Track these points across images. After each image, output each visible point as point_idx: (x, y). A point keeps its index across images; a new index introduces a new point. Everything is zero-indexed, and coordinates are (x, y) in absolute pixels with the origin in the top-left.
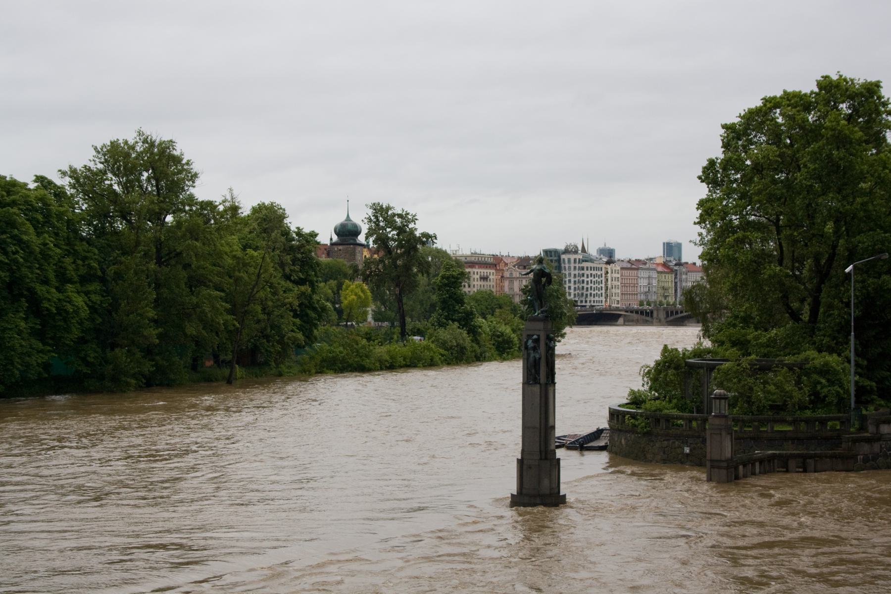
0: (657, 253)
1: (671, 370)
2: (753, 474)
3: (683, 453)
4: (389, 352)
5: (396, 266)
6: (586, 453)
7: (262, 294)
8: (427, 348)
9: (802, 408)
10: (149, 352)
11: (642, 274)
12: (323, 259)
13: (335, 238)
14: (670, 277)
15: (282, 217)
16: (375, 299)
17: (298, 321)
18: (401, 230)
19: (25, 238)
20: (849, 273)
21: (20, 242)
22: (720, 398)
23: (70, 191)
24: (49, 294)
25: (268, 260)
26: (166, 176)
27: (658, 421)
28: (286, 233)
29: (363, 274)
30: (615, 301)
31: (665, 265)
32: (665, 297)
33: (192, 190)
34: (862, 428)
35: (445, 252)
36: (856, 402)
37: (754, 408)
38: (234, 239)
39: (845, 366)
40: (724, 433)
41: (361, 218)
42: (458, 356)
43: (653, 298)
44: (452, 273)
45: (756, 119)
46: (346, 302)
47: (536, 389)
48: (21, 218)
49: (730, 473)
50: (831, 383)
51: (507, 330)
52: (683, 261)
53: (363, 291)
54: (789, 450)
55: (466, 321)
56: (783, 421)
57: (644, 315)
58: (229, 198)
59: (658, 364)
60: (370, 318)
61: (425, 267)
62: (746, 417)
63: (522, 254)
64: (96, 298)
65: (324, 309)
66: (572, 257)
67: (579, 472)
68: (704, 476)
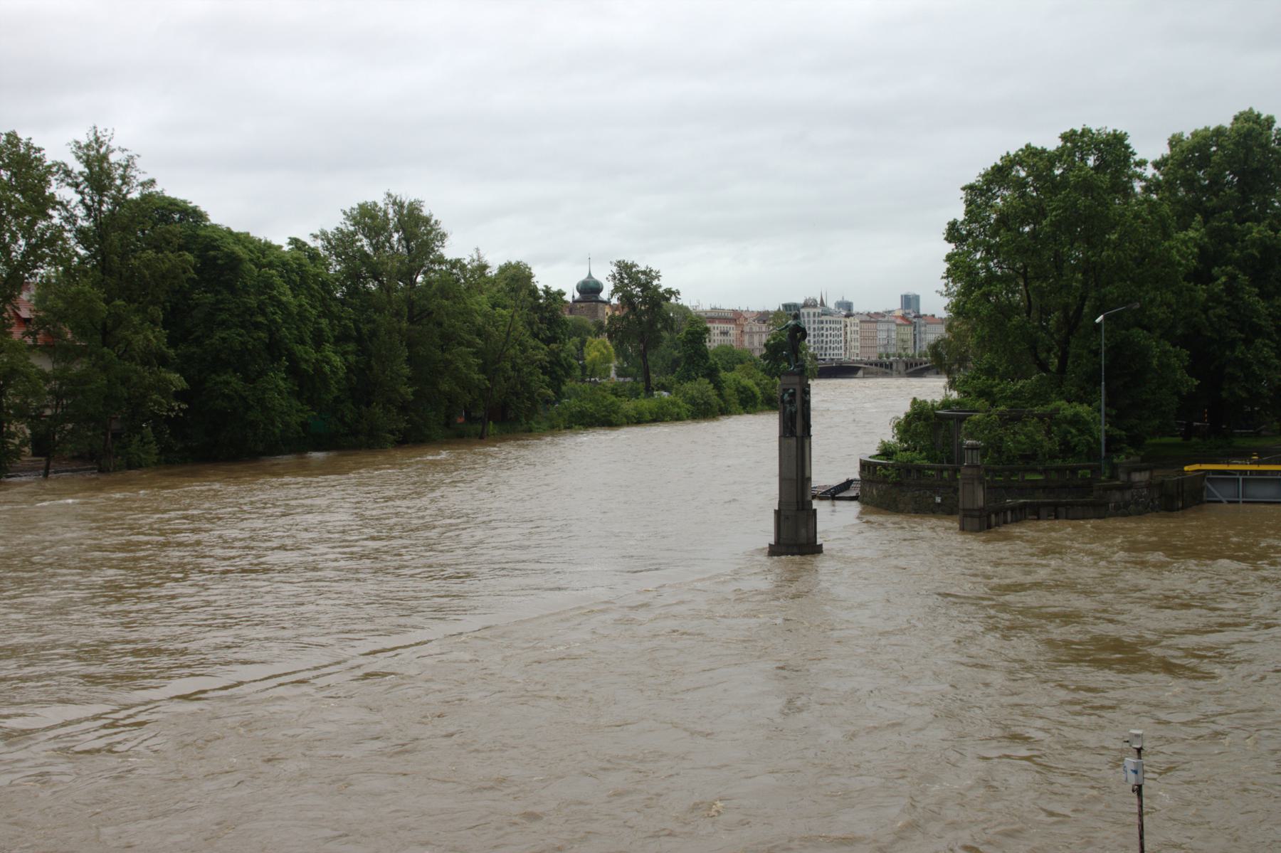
0: (895, 305)
1: (920, 422)
2: (1005, 522)
3: (934, 502)
4: (636, 408)
5: (641, 323)
6: (837, 503)
7: (512, 351)
8: (674, 404)
9: (1053, 457)
10: (404, 408)
11: (881, 327)
12: (568, 316)
13: (577, 295)
14: (910, 329)
15: (530, 276)
16: (618, 357)
17: (547, 378)
18: (646, 287)
19: (284, 299)
20: (1100, 324)
21: (280, 304)
22: (973, 448)
23: (323, 253)
24: (307, 353)
25: (516, 318)
26: (415, 236)
27: (909, 471)
28: (533, 291)
29: (608, 331)
30: (854, 354)
31: (903, 317)
32: (905, 349)
33: (442, 250)
34: (1113, 477)
35: (687, 308)
36: (1107, 451)
37: (1004, 457)
38: (483, 298)
39: (1094, 415)
40: (976, 483)
41: (605, 276)
42: (703, 411)
43: (892, 350)
44: (695, 329)
45: (999, 174)
46: (589, 358)
47: (793, 441)
48: (278, 280)
49: (982, 522)
50: (1081, 432)
51: (749, 383)
52: (922, 312)
53: (606, 347)
54: (1040, 498)
55: (712, 374)
56: (1034, 471)
57: (883, 367)
58: (475, 257)
59: (907, 416)
60: (613, 374)
61: (669, 324)
62: (997, 467)
63: (761, 309)
64: (351, 358)
65: (570, 366)
66: (812, 311)
67: (836, 522)
68: (956, 525)
